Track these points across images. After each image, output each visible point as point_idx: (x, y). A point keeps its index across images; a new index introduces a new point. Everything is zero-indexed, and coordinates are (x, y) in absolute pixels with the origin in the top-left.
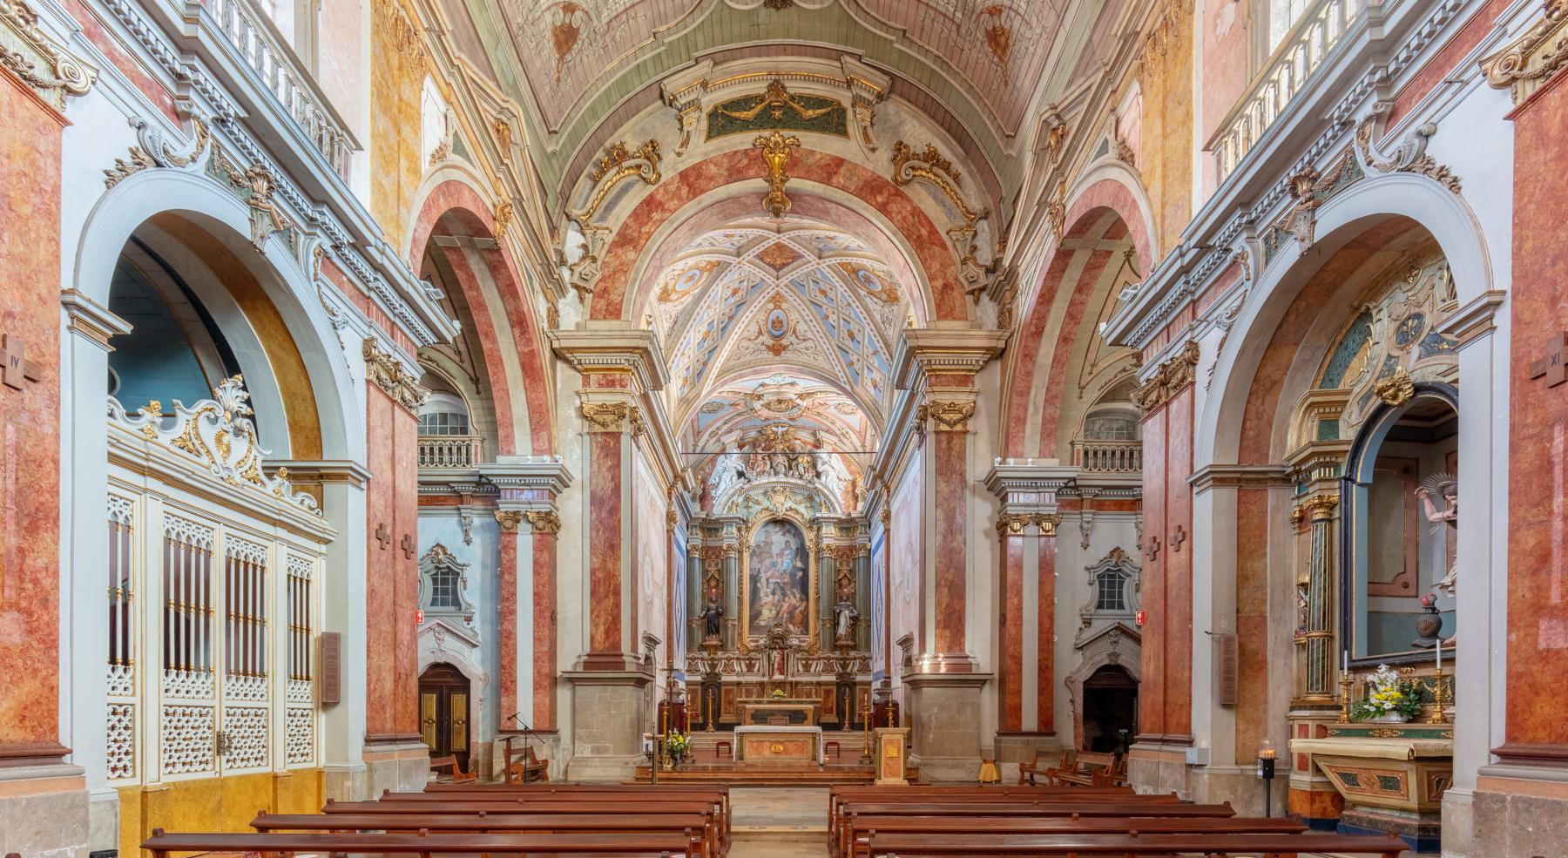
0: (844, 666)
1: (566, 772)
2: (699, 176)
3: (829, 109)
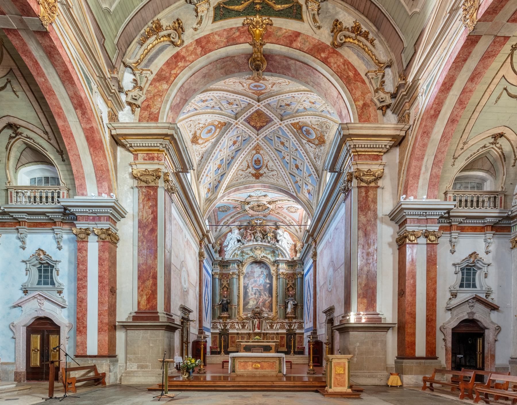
0: (290, 326)
1: (121, 379)
2: (208, 42)
3: (291, 5)
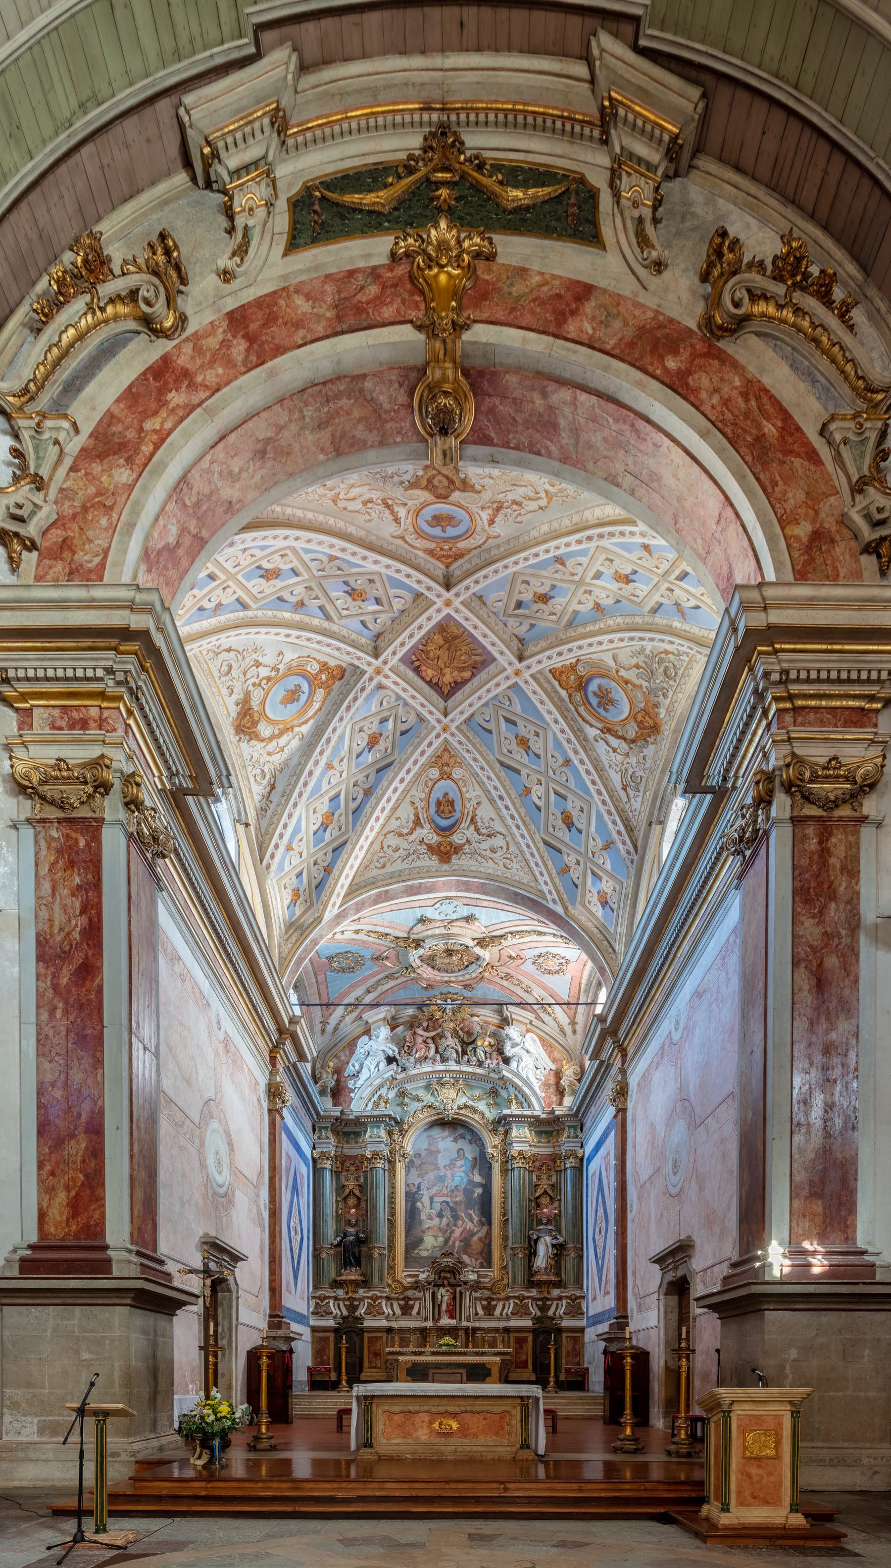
0: (544, 1309)
2: (271, 319)
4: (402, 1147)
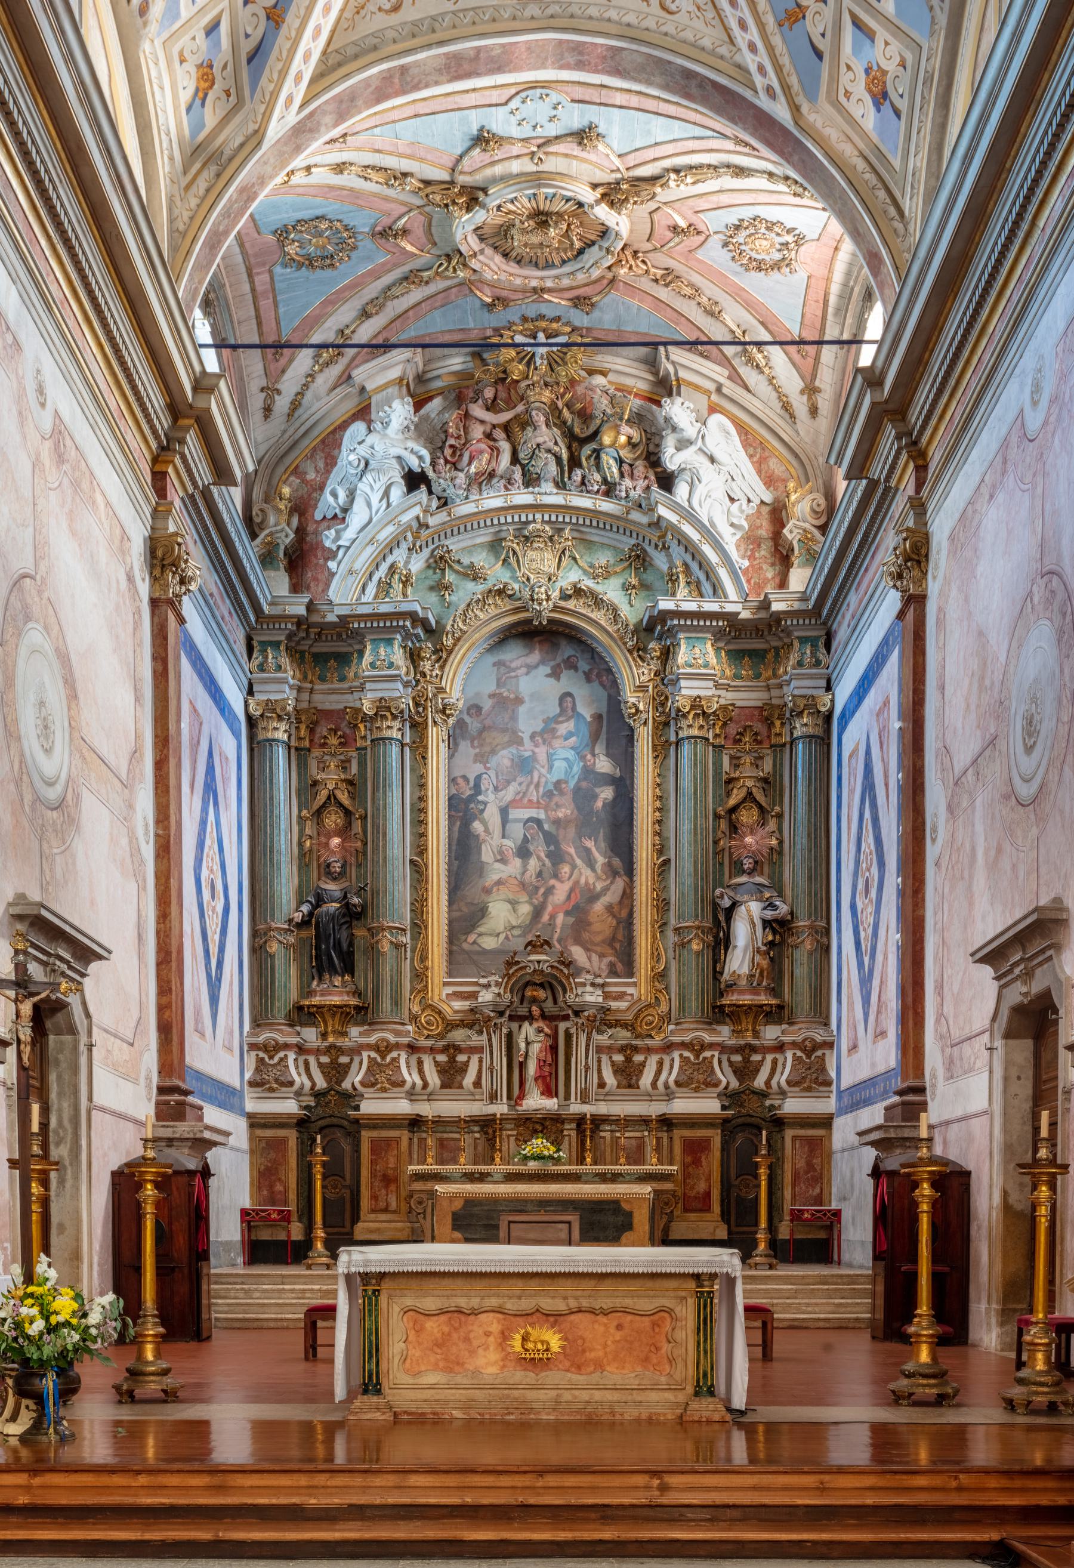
0: (745, 1071)
4: (441, 690)
